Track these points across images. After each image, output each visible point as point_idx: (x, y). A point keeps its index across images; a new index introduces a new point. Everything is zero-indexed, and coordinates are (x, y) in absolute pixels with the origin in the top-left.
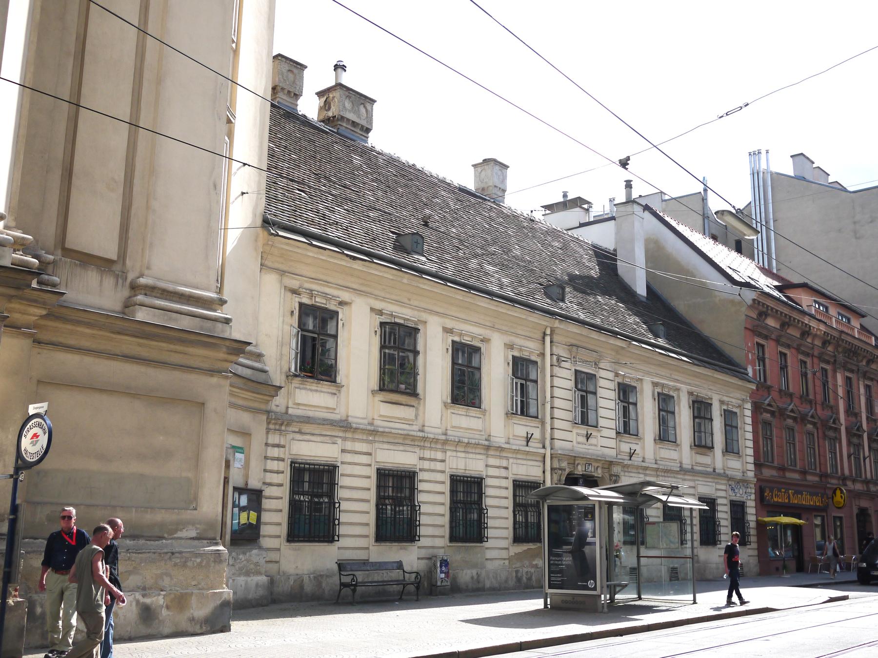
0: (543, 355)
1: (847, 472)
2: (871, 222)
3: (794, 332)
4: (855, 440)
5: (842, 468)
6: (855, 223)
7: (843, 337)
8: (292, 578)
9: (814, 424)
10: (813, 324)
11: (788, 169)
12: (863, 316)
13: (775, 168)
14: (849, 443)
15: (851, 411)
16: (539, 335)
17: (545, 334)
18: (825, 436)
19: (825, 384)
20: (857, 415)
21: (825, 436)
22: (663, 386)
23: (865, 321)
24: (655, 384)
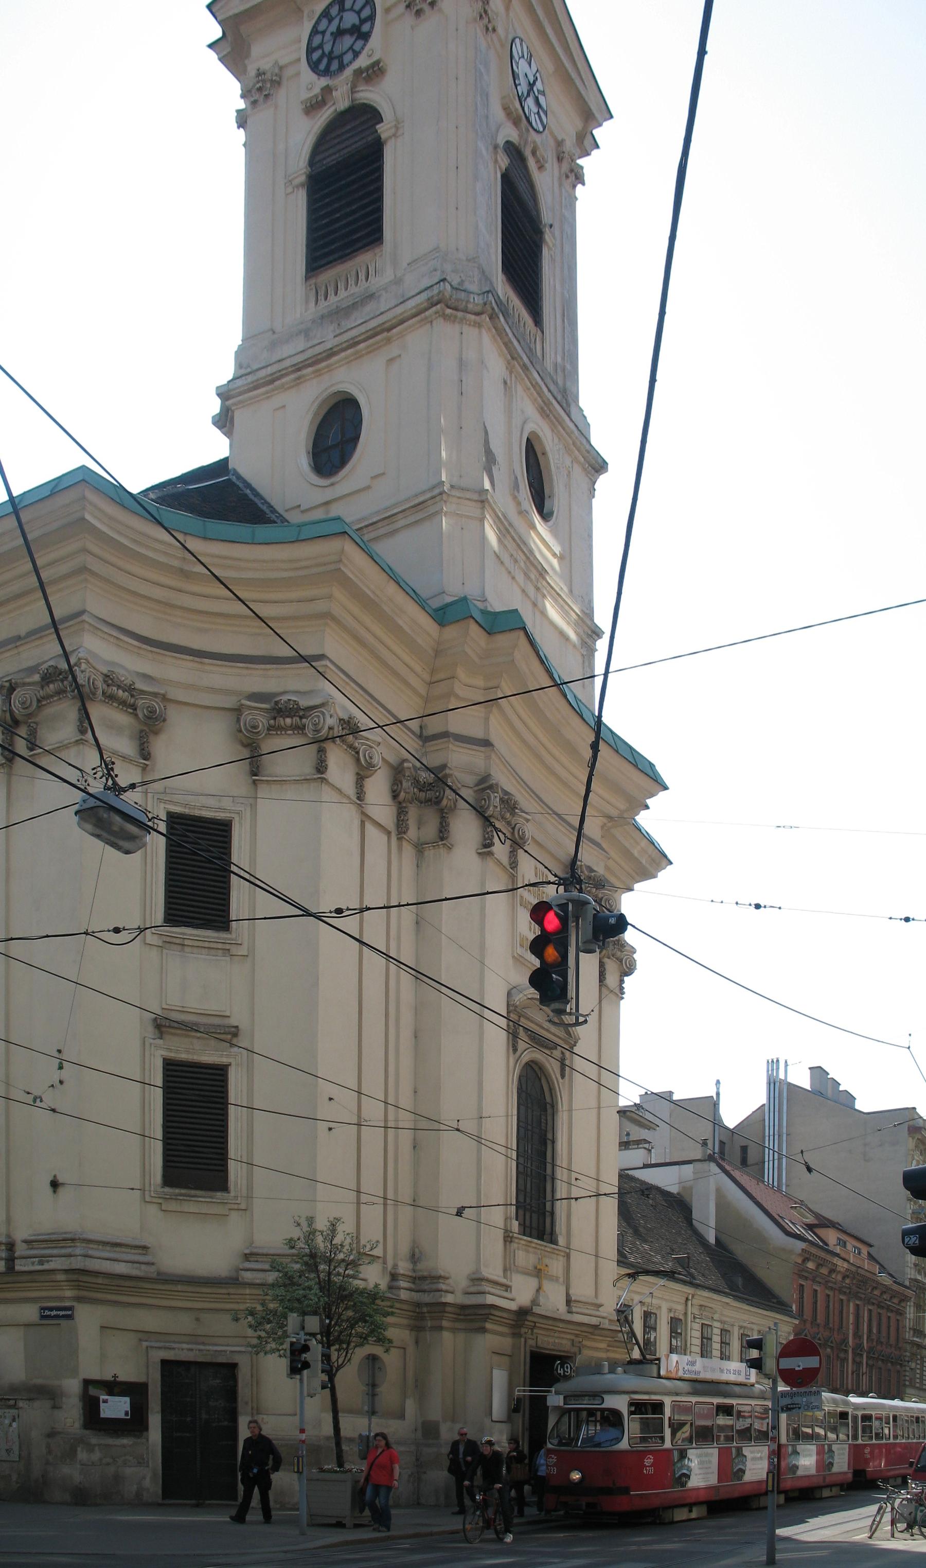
0: (686, 1314)
1: (850, 1386)
2: (880, 1145)
3: (824, 1271)
4: (858, 1359)
5: (847, 1383)
6: (865, 1145)
7: (860, 1271)
8: (14, 1477)
9: (832, 1348)
10: (839, 1262)
11: (803, 1080)
12: (871, 1246)
13: (792, 1079)
14: (854, 1361)
15: (857, 1335)
16: (683, 1300)
17: (687, 1299)
18: (838, 1357)
19: (841, 1312)
20: (861, 1337)
21: (838, 1357)
22: (745, 1327)
23: (872, 1250)
24: (741, 1327)
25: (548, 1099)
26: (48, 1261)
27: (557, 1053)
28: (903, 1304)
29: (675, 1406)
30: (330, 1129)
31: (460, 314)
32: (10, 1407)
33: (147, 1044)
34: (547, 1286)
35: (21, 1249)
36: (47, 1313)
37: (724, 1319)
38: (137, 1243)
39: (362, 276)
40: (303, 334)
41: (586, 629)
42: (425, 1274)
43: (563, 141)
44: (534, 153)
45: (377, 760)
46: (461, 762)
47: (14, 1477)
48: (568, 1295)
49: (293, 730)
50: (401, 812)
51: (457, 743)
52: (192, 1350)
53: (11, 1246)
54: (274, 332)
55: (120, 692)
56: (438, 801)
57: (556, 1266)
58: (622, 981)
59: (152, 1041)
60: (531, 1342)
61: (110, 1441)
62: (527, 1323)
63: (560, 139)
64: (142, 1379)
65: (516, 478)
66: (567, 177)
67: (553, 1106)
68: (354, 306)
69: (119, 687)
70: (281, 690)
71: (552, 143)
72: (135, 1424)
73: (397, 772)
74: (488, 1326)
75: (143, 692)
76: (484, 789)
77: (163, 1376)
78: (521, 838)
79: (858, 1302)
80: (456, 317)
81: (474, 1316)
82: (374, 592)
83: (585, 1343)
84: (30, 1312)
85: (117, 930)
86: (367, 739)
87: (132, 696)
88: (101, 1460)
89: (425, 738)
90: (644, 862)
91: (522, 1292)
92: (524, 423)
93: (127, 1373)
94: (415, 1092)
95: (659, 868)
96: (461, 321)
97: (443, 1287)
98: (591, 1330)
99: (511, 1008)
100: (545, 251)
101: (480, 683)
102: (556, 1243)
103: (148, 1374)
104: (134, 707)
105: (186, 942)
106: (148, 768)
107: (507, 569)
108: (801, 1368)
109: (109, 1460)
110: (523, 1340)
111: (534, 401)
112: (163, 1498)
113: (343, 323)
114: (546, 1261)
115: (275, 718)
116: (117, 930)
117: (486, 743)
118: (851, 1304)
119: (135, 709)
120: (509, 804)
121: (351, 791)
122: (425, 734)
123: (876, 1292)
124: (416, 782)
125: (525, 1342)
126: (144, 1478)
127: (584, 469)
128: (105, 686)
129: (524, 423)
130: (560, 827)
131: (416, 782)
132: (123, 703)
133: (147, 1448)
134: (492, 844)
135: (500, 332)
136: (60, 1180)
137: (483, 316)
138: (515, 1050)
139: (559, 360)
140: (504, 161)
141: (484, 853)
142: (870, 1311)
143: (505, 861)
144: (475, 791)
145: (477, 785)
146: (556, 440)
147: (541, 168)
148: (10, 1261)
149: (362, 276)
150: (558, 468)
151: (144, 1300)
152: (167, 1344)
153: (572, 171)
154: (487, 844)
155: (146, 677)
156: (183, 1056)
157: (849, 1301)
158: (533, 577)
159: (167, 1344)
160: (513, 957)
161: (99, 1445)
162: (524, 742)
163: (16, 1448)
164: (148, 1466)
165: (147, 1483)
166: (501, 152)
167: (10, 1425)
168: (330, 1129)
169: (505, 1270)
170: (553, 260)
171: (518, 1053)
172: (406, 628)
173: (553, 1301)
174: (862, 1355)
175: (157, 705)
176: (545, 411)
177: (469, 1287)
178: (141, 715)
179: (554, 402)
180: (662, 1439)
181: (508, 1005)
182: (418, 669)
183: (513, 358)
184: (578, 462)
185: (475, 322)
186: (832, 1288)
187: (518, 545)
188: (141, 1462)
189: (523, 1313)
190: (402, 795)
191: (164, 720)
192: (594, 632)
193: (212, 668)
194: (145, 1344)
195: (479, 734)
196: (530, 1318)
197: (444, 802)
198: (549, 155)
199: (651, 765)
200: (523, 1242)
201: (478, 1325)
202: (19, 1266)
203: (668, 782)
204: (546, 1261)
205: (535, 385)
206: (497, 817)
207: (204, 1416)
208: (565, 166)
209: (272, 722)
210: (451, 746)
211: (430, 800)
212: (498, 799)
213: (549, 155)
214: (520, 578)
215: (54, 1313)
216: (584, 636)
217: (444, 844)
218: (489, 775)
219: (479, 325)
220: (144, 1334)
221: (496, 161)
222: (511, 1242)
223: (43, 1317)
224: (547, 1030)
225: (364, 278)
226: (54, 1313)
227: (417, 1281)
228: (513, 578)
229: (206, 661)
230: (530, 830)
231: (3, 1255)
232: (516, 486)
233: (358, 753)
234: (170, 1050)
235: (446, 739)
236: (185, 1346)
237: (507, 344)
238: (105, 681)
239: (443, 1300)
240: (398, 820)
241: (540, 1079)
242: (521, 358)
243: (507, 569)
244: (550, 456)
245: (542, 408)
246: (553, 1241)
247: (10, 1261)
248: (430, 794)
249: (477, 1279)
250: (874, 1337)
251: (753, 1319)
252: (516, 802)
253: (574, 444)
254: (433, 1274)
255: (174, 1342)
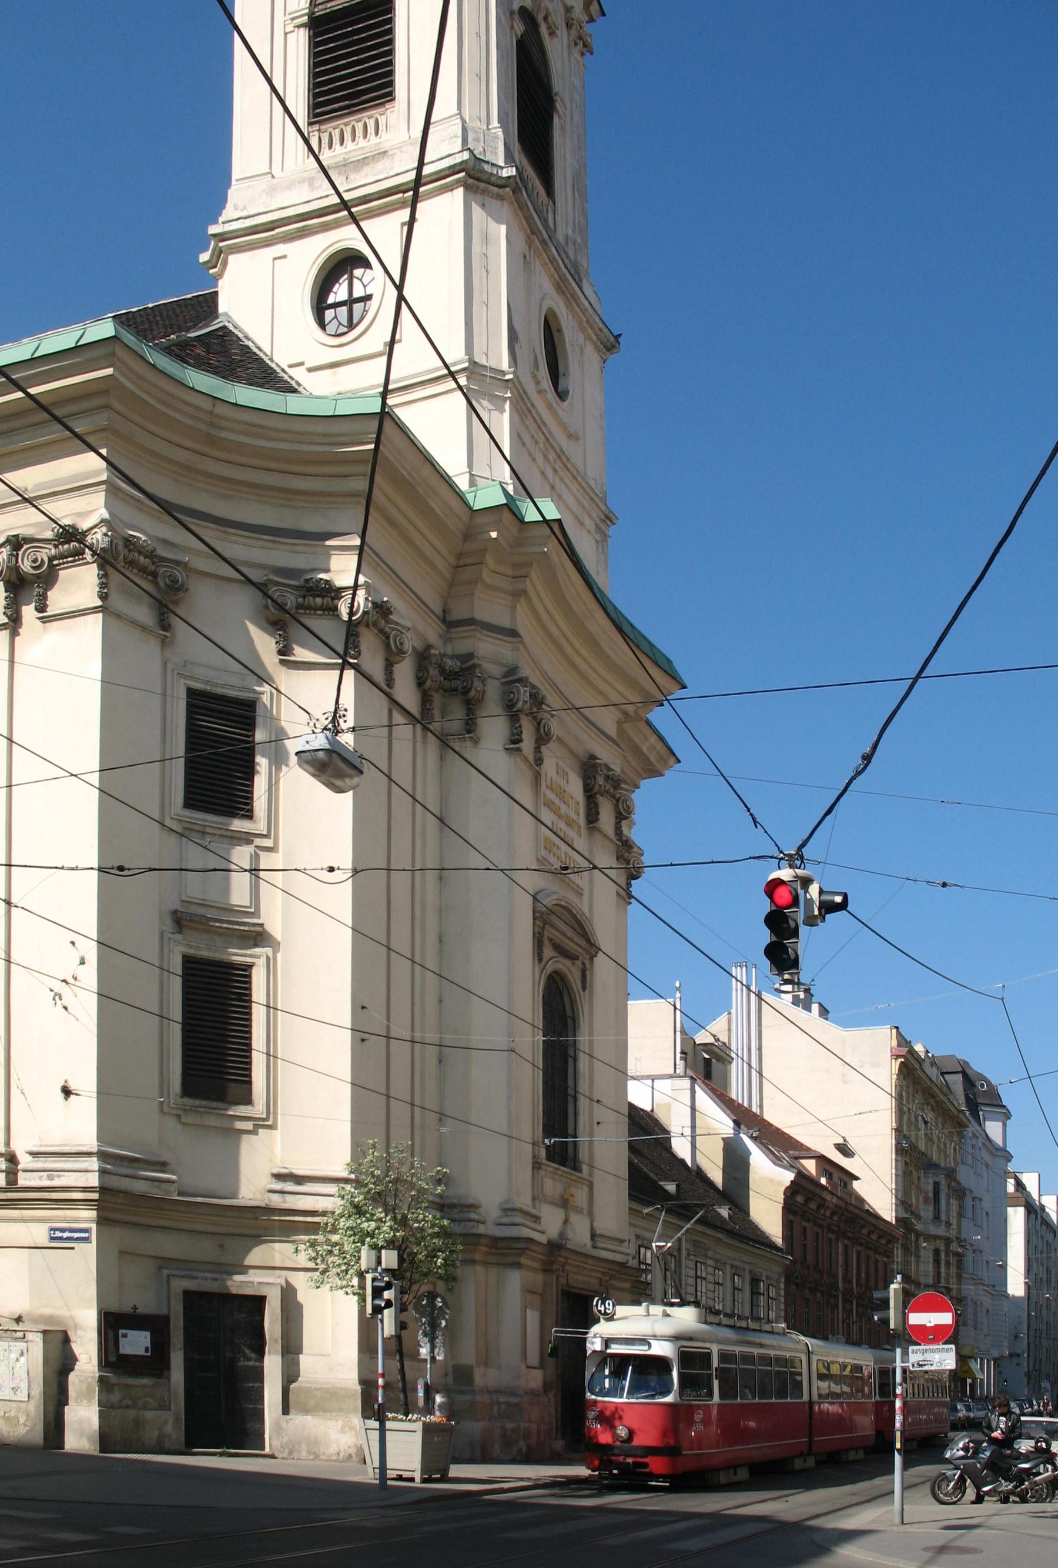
3: (813, 1205)
8: (22, 1419)
9: (822, 1292)
14: (844, 1307)
15: (847, 1280)
20: (850, 1282)
25: (569, 1013)
26: (59, 1176)
27: (578, 963)
28: (890, 1246)
29: (724, 1357)
30: (363, 1040)
31: (483, 185)
32: (17, 1339)
33: (166, 938)
34: (574, 1218)
35: (25, 1161)
36: (58, 1234)
37: (717, 1256)
38: (156, 1159)
39: (371, 129)
40: (306, 183)
41: (600, 514)
42: (455, 1201)
43: (572, 7)
44: (546, 19)
45: (408, 646)
46: (489, 650)
47: (22, 1419)
48: (592, 1228)
49: (324, 610)
50: (426, 700)
51: (484, 632)
52: (216, 1280)
53: (12, 1159)
54: (273, 177)
55: (142, 558)
56: (466, 691)
57: (580, 1196)
58: (629, 885)
59: (171, 936)
60: (562, 1280)
61: (130, 1381)
62: (560, 1259)
63: (569, 5)
64: (164, 1311)
65: (536, 357)
66: (576, 44)
67: (575, 1020)
68: (364, 161)
69: (140, 553)
70: (308, 567)
71: (562, 9)
72: (155, 1363)
73: (423, 657)
74: (523, 1260)
75: (163, 559)
76: (511, 682)
77: (185, 1308)
78: (546, 734)
79: (846, 1242)
80: (478, 188)
81: (505, 1251)
82: (409, 473)
83: (612, 1282)
84: (39, 1234)
85: (331, 869)
86: (397, 624)
87: (153, 563)
88: (120, 1401)
89: (449, 623)
90: (652, 759)
91: (551, 1223)
92: (543, 298)
93: (147, 1303)
94: (441, 1001)
95: (666, 765)
96: (484, 192)
97: (473, 1216)
98: (617, 1268)
99: (537, 915)
100: (556, 120)
101: (509, 571)
102: (580, 1171)
103: (169, 1308)
104: (154, 575)
105: (208, 830)
106: (167, 640)
107: (528, 450)
108: (932, 1324)
109: (128, 1402)
110: (555, 1277)
111: (551, 277)
112: (101, 1452)
113: (352, 177)
114: (573, 1190)
115: (304, 597)
116: (331, 869)
117: (513, 633)
118: (840, 1245)
119: (155, 577)
120: (538, 700)
121: (379, 677)
122: (448, 618)
123: (864, 1231)
124: (442, 669)
125: (557, 1278)
126: (166, 1422)
127: (596, 347)
128: (126, 551)
129: (543, 298)
130: (580, 723)
131: (442, 669)
132: (143, 570)
133: (169, 1390)
134: (520, 741)
135: (522, 207)
136: (72, 1087)
137: (508, 189)
138: (540, 960)
139: (570, 233)
140: (520, 28)
141: (511, 749)
142: (858, 1252)
143: (531, 758)
144: (503, 684)
145: (503, 677)
146: (571, 317)
147: (552, 34)
148: (12, 1174)
149: (371, 129)
150: (572, 345)
151: (162, 1223)
152: (190, 1273)
153: (580, 38)
154: (515, 739)
155: (166, 542)
156: (204, 954)
157: (837, 1240)
158: (551, 458)
159: (190, 1273)
160: (538, 859)
161: (119, 1385)
162: (544, 628)
163: (24, 1386)
164: (170, 1409)
165: (169, 1428)
166: (516, 17)
167: (17, 1360)
168: (363, 1040)
169: (534, 1199)
170: (563, 128)
171: (543, 963)
172: (437, 510)
173: (579, 1235)
174: (851, 1302)
175: (180, 575)
176: (561, 287)
177: (500, 1217)
178: (162, 584)
179: (570, 278)
180: (710, 1394)
181: (534, 911)
182: (445, 552)
183: (532, 233)
184: (591, 340)
185: (498, 195)
186: (821, 1226)
187: (539, 426)
188: (164, 1406)
189: (555, 1247)
190: (428, 683)
191: (187, 590)
192: (607, 517)
193: (234, 538)
194: (165, 1272)
195: (505, 622)
196: (563, 1253)
197: (472, 693)
198: (559, 20)
199: (669, 661)
200: (550, 1169)
201: (511, 1260)
202: (23, 1180)
203: (687, 682)
204: (573, 1190)
205: (552, 261)
206: (528, 712)
207: (228, 1354)
208: (574, 33)
209: (300, 600)
210: (478, 634)
211: (456, 690)
212: (528, 694)
213: (559, 20)
214: (540, 459)
215: (66, 1235)
216: (598, 522)
217: (471, 738)
218: (517, 667)
219: (500, 198)
220: (164, 1262)
221: (512, 28)
222: (539, 1168)
223: (52, 1239)
224: (571, 939)
225: (373, 131)
226: (66, 1235)
227: (446, 1209)
228: (534, 460)
229: (231, 530)
230: (556, 729)
231: (3, 1167)
232: (536, 366)
233: (388, 638)
234: (190, 947)
235: (473, 627)
236: (209, 1275)
237: (528, 219)
238: (126, 546)
239: (475, 1231)
240: (423, 709)
241: (562, 996)
242: (541, 233)
243: (528, 450)
244: (565, 331)
245: (558, 285)
246: (577, 1168)
247: (12, 1174)
248: (455, 684)
249: (508, 1210)
250: (863, 1282)
251: (744, 1258)
252: (544, 697)
253: (588, 321)
254: (463, 1202)
255: (196, 1270)
